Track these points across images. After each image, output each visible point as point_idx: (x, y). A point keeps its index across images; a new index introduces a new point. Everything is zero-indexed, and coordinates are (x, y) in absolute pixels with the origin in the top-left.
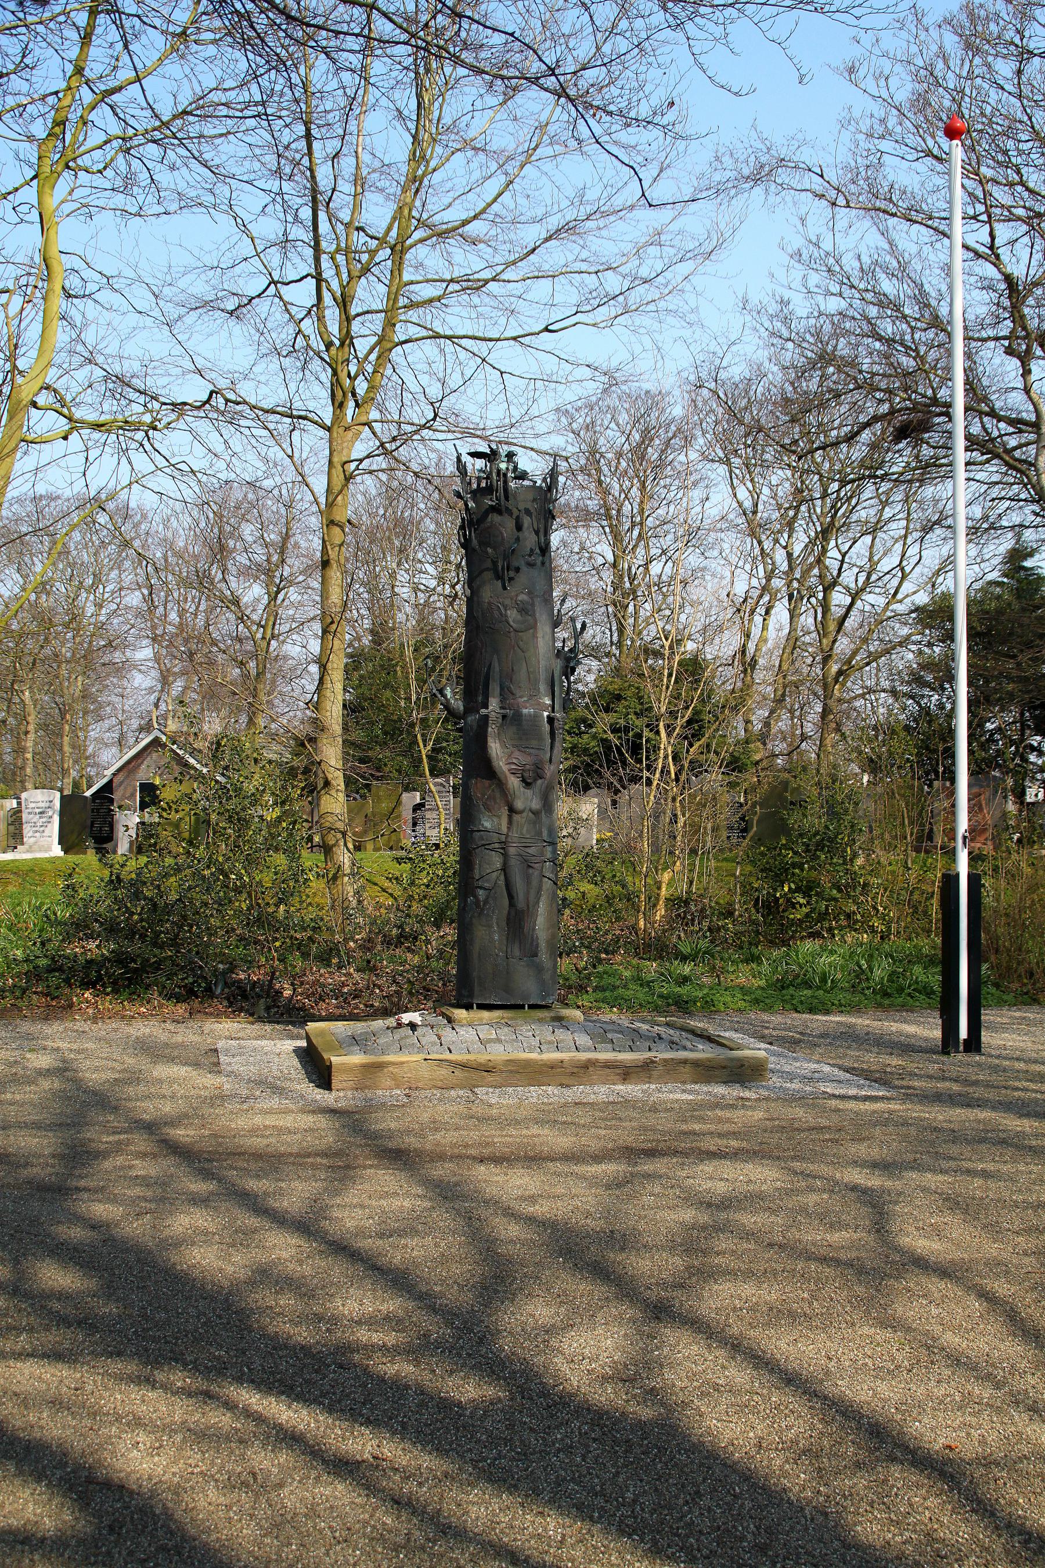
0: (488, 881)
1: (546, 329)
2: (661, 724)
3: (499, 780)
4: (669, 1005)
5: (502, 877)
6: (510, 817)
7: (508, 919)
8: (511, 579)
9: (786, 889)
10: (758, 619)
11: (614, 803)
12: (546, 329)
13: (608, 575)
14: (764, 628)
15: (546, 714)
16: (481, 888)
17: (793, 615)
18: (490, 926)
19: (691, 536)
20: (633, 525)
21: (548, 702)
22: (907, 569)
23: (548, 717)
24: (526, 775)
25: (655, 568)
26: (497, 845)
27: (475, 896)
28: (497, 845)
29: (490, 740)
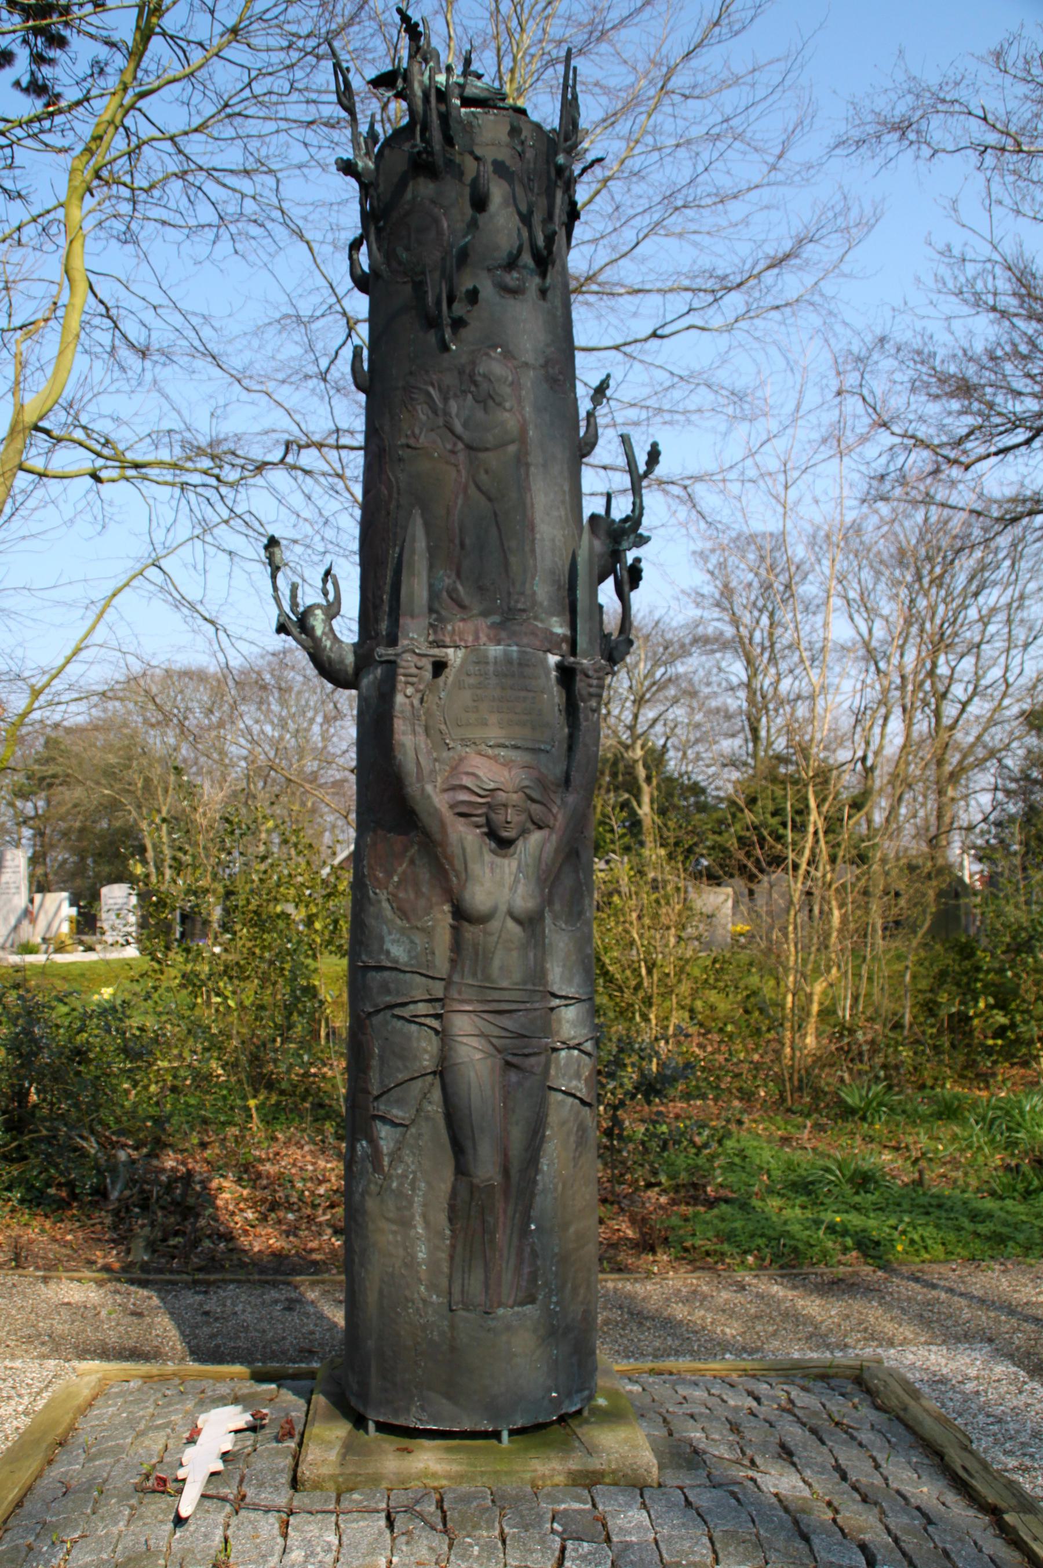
0: (400, 1102)
1: (654, 335)
2: (811, 789)
3: (427, 834)
4: (845, 1250)
5: (437, 1095)
6: (456, 930)
7: (452, 1209)
8: (458, 324)
9: (982, 1005)
10: (877, 730)
11: (751, 893)
12: (654, 335)
13: (742, 694)
14: (883, 736)
15: (553, 659)
16: (384, 1119)
17: (909, 725)
18: (406, 1224)
19: (818, 656)
20: (763, 649)
21: (560, 629)
22: (1011, 680)
23: (560, 667)
24: (498, 818)
25: (785, 685)
26: (422, 1008)
27: (373, 1142)
28: (422, 1008)
29: (400, 725)
